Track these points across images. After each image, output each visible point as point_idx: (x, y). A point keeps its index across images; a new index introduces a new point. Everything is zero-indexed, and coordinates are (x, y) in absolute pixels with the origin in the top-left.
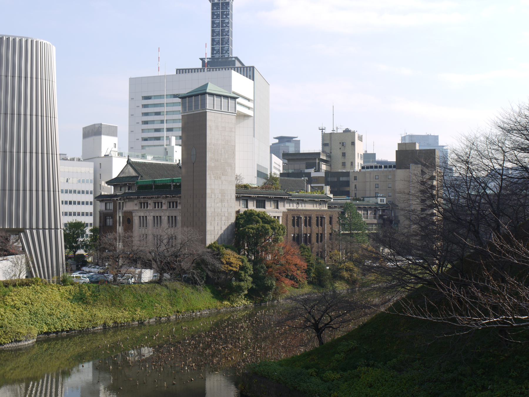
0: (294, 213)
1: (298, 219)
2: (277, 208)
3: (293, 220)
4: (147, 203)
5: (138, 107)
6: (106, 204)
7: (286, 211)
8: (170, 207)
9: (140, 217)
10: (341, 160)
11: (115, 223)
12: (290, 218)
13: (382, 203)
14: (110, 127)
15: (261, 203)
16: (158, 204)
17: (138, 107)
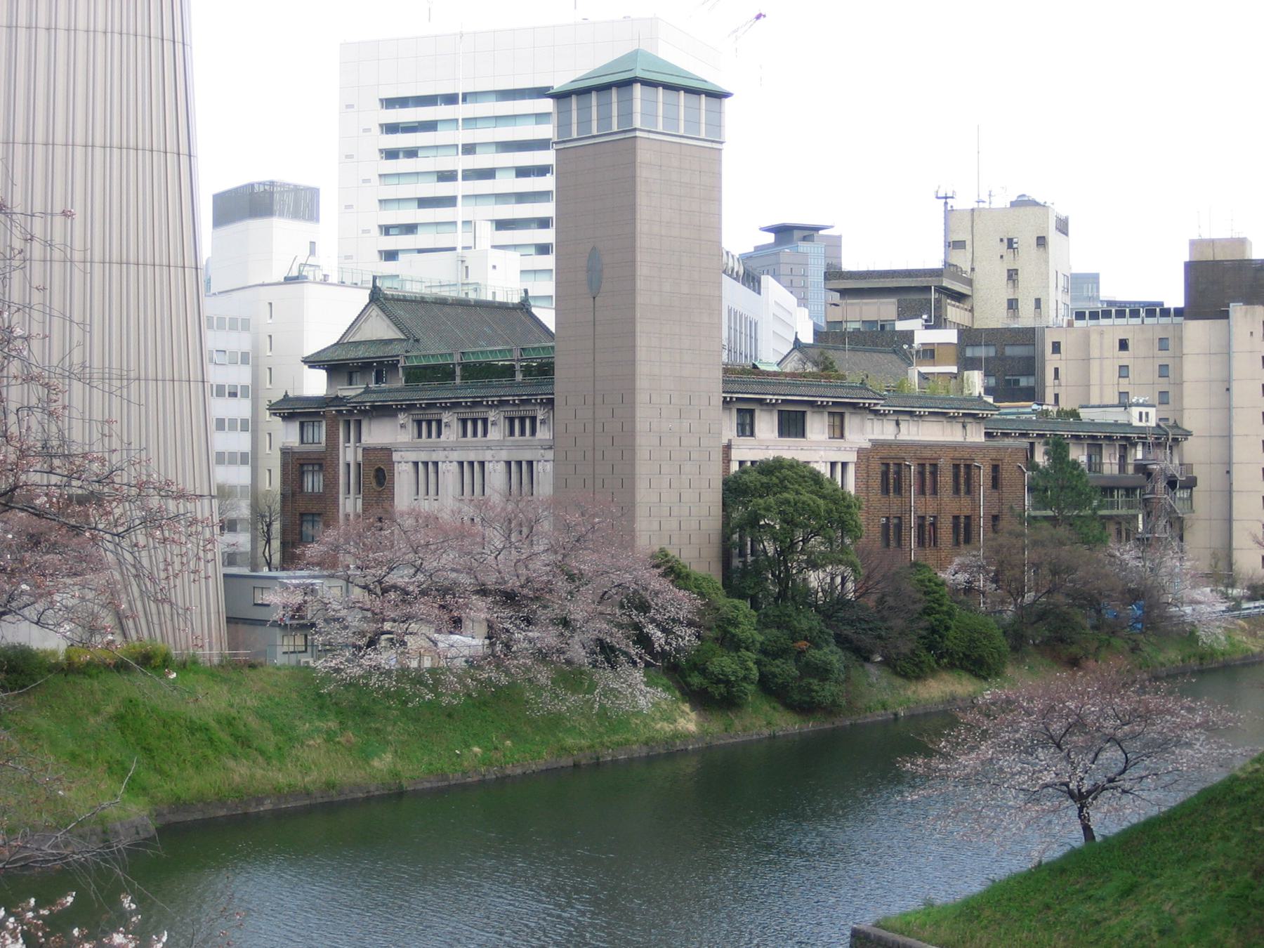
0: (885, 453)
1: (898, 473)
2: (842, 436)
3: (885, 474)
4: (439, 422)
5: (366, 130)
6: (302, 425)
7: (868, 445)
8: (512, 433)
9: (416, 464)
10: (1005, 293)
11: (331, 484)
12: (877, 469)
13: (1143, 424)
14: (296, 190)
15: (792, 424)
16: (473, 423)
17: (367, 130)
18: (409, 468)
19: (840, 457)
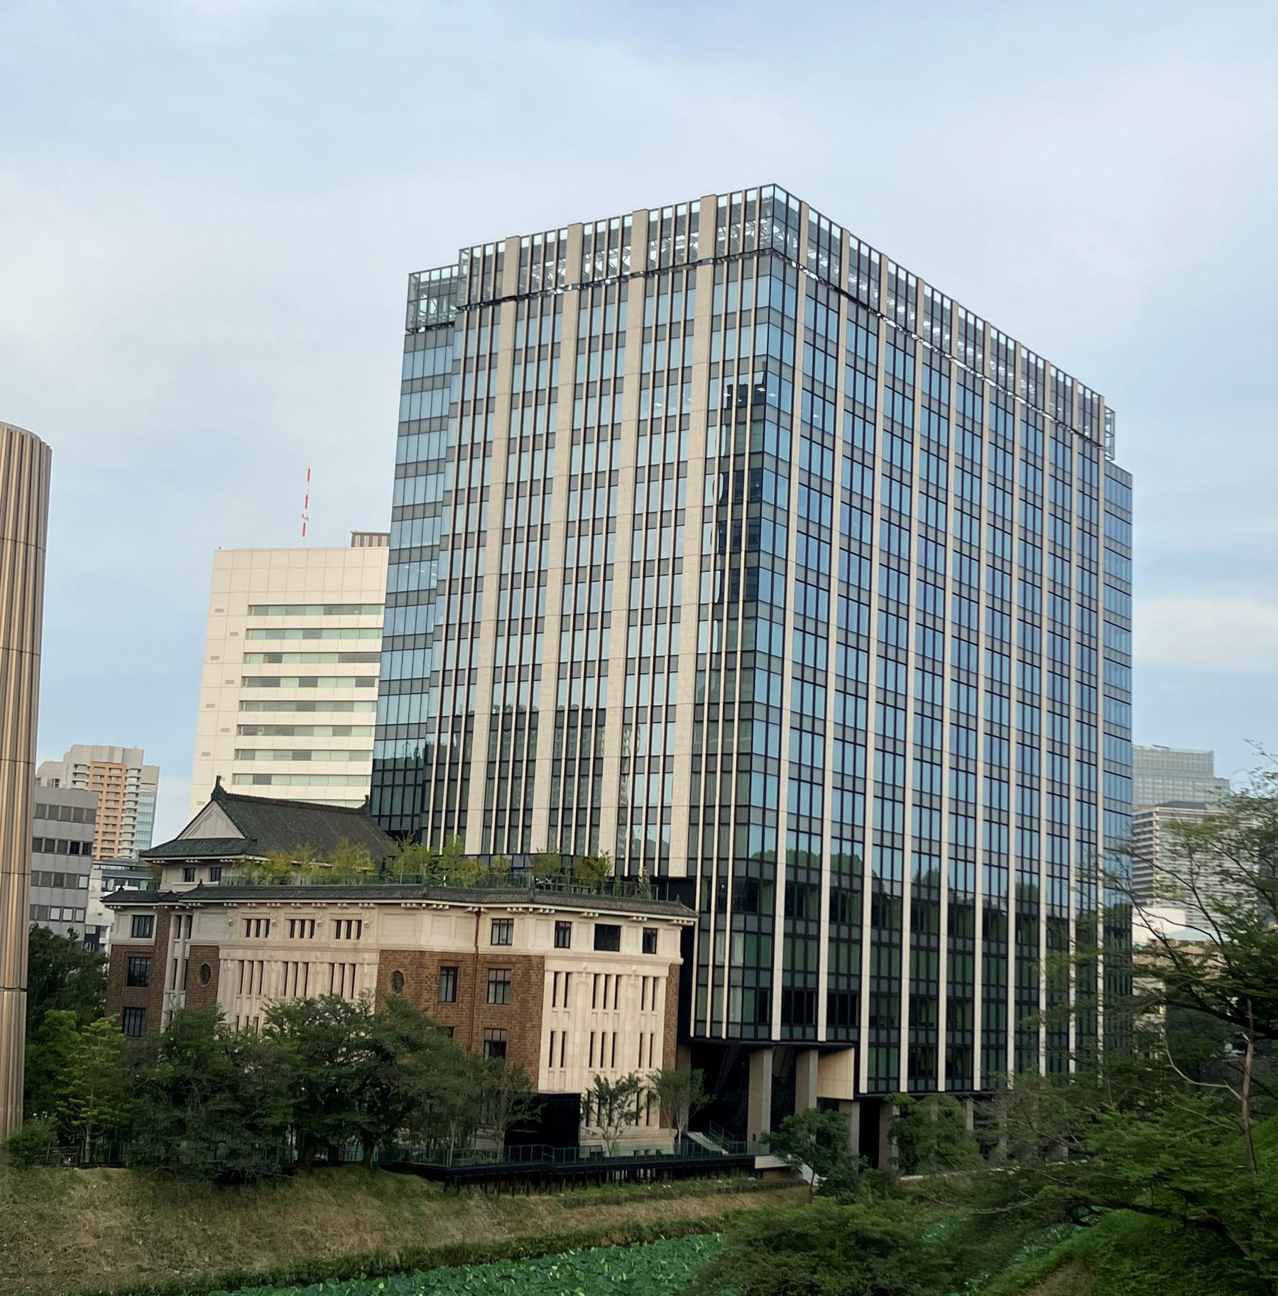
18: (233, 966)
19: (650, 971)
